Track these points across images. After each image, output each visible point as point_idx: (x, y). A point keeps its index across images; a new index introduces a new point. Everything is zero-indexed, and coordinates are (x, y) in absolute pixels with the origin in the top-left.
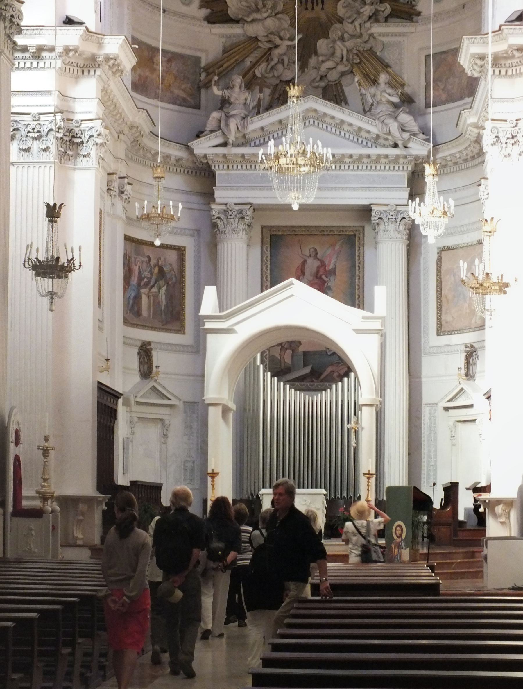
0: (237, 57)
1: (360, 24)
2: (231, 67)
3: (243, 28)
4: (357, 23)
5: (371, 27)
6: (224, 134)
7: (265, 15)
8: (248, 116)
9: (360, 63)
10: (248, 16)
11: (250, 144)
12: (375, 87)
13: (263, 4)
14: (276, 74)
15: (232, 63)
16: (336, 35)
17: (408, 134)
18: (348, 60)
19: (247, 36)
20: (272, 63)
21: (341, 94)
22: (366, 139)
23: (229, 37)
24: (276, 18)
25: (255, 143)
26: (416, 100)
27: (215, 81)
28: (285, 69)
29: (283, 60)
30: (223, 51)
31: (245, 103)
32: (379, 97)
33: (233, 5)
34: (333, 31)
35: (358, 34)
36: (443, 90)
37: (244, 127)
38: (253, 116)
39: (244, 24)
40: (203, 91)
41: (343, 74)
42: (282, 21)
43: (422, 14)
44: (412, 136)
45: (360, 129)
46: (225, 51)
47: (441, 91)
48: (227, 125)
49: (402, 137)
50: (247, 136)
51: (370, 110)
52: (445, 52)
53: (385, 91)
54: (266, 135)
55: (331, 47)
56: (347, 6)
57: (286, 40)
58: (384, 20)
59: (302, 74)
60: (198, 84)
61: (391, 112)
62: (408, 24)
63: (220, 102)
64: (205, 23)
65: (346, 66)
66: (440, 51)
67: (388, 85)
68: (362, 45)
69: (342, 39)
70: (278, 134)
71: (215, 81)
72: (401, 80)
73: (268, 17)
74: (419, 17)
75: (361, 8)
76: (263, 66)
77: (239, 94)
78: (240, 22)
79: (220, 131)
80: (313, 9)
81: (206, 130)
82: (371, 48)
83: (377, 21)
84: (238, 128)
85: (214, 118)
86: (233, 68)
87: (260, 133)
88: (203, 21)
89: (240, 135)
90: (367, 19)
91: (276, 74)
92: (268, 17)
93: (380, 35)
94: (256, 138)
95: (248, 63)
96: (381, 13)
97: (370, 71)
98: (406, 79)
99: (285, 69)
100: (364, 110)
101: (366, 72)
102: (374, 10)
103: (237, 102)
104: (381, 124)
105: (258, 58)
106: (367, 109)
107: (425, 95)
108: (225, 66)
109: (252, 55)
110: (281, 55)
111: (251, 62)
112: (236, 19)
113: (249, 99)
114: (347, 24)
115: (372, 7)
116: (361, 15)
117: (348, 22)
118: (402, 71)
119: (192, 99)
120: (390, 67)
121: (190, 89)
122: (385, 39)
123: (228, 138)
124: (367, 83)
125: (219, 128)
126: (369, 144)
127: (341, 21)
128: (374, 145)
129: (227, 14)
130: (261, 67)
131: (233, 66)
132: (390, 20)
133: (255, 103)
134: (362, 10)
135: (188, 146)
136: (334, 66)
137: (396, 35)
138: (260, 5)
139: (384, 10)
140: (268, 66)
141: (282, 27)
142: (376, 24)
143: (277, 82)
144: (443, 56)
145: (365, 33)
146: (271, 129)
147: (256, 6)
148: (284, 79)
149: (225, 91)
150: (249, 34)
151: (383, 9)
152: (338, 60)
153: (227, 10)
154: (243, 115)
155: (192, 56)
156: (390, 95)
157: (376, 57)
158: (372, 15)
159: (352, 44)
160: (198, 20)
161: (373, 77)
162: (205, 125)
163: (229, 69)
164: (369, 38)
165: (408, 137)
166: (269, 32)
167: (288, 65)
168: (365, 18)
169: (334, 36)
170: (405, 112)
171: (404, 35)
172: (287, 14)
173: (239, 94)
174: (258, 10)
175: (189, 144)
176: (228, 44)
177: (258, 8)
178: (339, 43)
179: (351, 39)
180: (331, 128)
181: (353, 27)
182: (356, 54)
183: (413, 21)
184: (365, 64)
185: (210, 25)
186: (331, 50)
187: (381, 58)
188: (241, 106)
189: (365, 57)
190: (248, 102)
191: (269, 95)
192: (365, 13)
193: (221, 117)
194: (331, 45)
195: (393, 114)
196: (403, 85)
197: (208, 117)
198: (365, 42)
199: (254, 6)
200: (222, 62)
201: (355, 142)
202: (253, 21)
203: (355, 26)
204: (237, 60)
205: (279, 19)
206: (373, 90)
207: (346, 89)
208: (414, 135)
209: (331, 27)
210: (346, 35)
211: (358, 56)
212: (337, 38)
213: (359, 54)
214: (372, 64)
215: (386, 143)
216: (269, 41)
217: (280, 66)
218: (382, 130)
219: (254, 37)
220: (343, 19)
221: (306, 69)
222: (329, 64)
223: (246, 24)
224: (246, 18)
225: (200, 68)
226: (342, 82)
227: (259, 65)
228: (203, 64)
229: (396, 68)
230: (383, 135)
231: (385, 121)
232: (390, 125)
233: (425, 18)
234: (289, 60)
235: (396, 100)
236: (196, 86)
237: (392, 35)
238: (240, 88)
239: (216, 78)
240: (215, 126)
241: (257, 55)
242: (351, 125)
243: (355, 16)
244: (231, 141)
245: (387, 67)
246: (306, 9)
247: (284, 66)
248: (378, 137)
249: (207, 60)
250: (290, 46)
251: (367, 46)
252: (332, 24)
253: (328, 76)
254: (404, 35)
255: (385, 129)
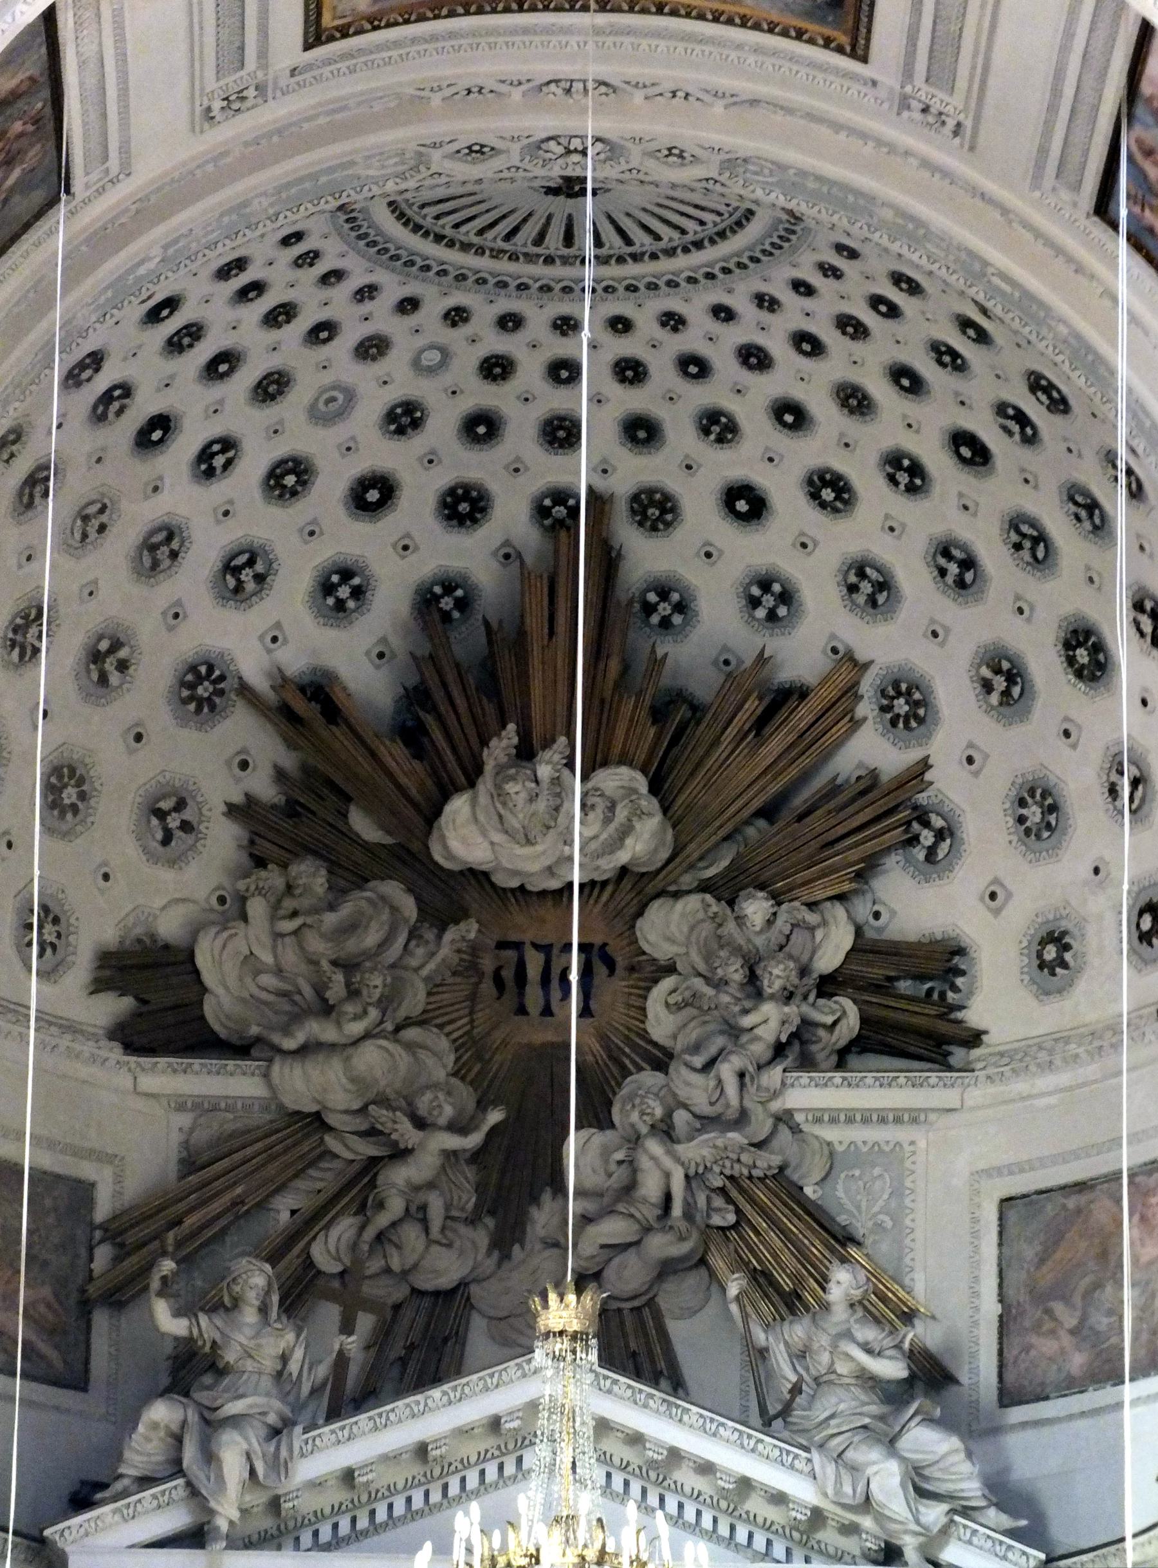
0: (239, 1190)
1: (741, 1075)
2: (216, 1229)
3: (266, 1076)
4: (727, 1070)
5: (783, 1084)
6: (193, 1491)
7: (356, 1028)
8: (294, 1424)
9: (735, 1227)
10: (286, 1031)
11: (297, 1539)
12: (807, 1320)
13: (348, 984)
14: (396, 1264)
15: (218, 1217)
16: (642, 1113)
17: (944, 1507)
18: (688, 1215)
19: (281, 1107)
20: (382, 1220)
21: (658, 1350)
22: (767, 1527)
23: (204, 1107)
24: (397, 1041)
25: (316, 1534)
26: (964, 1377)
27: (164, 1279)
28: (430, 1242)
29: (423, 1208)
30: (182, 1161)
31: (279, 1374)
32: (825, 1358)
33: (227, 988)
34: (631, 1097)
35: (732, 1114)
36: (1073, 1332)
37: (279, 1466)
38: (311, 1426)
39: (270, 1061)
40: (101, 1319)
41: (667, 1269)
42: (422, 1054)
43: (984, 1038)
44: (957, 1518)
45: (745, 1484)
46: (190, 1163)
47: (1066, 1340)
48: (210, 1457)
49: (918, 1522)
50: (287, 1506)
51: (786, 1411)
52: (1080, 1186)
53: (848, 1335)
54: (362, 1505)
55: (620, 1163)
56: (686, 1004)
57: (440, 1128)
58: (834, 1058)
59: (499, 1265)
60: (83, 1291)
61: (874, 1417)
62: (933, 1077)
63: (165, 1366)
64: (115, 1052)
65: (682, 1239)
66: (1062, 1181)
67: (860, 1313)
68: (744, 1158)
69: (665, 1131)
70: (409, 1500)
71: (164, 1279)
72: (902, 1294)
73: (367, 1036)
74: (976, 1053)
75: (746, 1012)
76: (343, 1229)
77: (257, 1335)
78: (254, 1052)
79: (180, 1481)
80: (547, 1011)
81: (121, 1476)
82: (782, 1169)
83: (807, 1063)
84: (252, 1472)
85: (155, 1426)
86: (224, 1231)
87: (337, 1495)
88: (104, 1042)
89: (258, 1499)
90: (768, 1054)
91: (396, 1264)
92: (367, 1036)
93: (818, 1120)
94: (319, 1516)
95: (285, 1216)
96: (822, 1033)
97: (775, 1256)
98: (919, 1288)
99: (430, 1242)
100: (763, 1410)
101: (759, 1261)
102: (797, 1021)
103: (249, 1365)
104: (831, 1469)
105: (323, 1197)
106: (773, 1408)
107: (1001, 1353)
108: (190, 1221)
109: (300, 1184)
110: (417, 1188)
111: (293, 1212)
112: (234, 1040)
113: (298, 1354)
114: (684, 1071)
115: (786, 1009)
116: (744, 1038)
117: (688, 1065)
118: (907, 1260)
119: (56, 1347)
120: (858, 1244)
121: (49, 1306)
122: (830, 1134)
123: (212, 1512)
124: (763, 1306)
125: (176, 1468)
126: (779, 1550)
127: (661, 1060)
128: (798, 1554)
129: (202, 1018)
130: (334, 1233)
131: (223, 1222)
132: (853, 1060)
133: (323, 1371)
134: (747, 1021)
135: (42, 1541)
136: (635, 1238)
137: (883, 1120)
138: (337, 989)
139: (835, 1023)
140: (362, 1228)
141: (423, 1080)
142: (805, 1077)
143: (399, 1293)
144: (1072, 1202)
145: (760, 1108)
146: (381, 1478)
147: (320, 990)
148: (426, 1283)
149: (203, 1319)
150: (291, 1103)
151: (829, 1020)
152: (651, 1214)
153: (201, 1003)
154: (272, 1419)
155: (58, 1177)
156: (869, 1351)
157: (799, 1203)
158: (789, 1042)
159: (706, 1152)
160: (94, 1037)
161: (786, 1284)
162: (117, 1455)
163: (209, 1233)
164: (775, 1126)
165: (944, 1520)
166: (371, 1095)
167: (443, 1229)
168: (760, 1049)
169: (635, 1117)
170: (929, 1421)
171: (914, 1121)
172: (440, 1027)
173: (257, 1335)
174: (327, 1010)
175: (47, 1533)
176: (202, 1136)
177: (326, 1001)
178: (654, 1146)
179: (700, 1131)
180: (627, 1483)
181: (712, 1083)
182: (722, 1191)
183: (950, 1068)
184: (757, 1233)
185: (133, 1059)
186: (620, 1175)
187: (819, 1207)
188: (266, 1382)
189: (752, 1201)
190: (294, 1367)
191: (367, 1348)
192: (758, 1031)
193: (184, 1423)
194: (620, 1155)
195: (881, 1425)
196: (908, 1316)
197: (131, 1420)
198: (760, 1145)
199: (308, 991)
200: (182, 1207)
201: (720, 1540)
202: (304, 1051)
203: (720, 1081)
204: (238, 1202)
205: (410, 1047)
206: (797, 1331)
207: (677, 1329)
208: (966, 1512)
209: (619, 1085)
210: (681, 1118)
211: (729, 1200)
212: (644, 1130)
213: (734, 1193)
214: (783, 1232)
215: (850, 1544)
216: (371, 1133)
217: (411, 1234)
218: (838, 1491)
219: (309, 1115)
220: (670, 1055)
221: (516, 1248)
222: (613, 1229)
223: (277, 1059)
224: (276, 1038)
225: (93, 1227)
226: (658, 1300)
227: (327, 1227)
228: (102, 1212)
229: (883, 1248)
230: (839, 1511)
231: (850, 1454)
232: (870, 1471)
233: (1002, 1054)
234: (448, 1207)
235: (893, 1369)
236: (74, 1296)
237: (867, 1118)
238: (263, 1310)
239: (168, 1266)
240: (160, 1458)
241: (319, 1185)
242: (706, 1468)
243: (720, 1041)
244: (223, 1525)
245: (844, 1246)
246: (522, 1010)
247: (427, 1230)
248: (817, 1517)
249: (117, 1194)
250: (455, 1153)
251: (767, 1161)
252: (626, 1073)
253: (609, 1274)
254: (913, 1117)
255: (847, 1489)
